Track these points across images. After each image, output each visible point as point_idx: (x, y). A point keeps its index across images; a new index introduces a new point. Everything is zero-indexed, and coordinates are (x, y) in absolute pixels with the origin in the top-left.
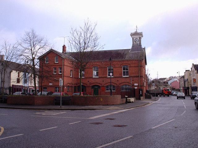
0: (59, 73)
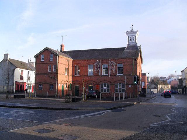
0: (54, 71)
